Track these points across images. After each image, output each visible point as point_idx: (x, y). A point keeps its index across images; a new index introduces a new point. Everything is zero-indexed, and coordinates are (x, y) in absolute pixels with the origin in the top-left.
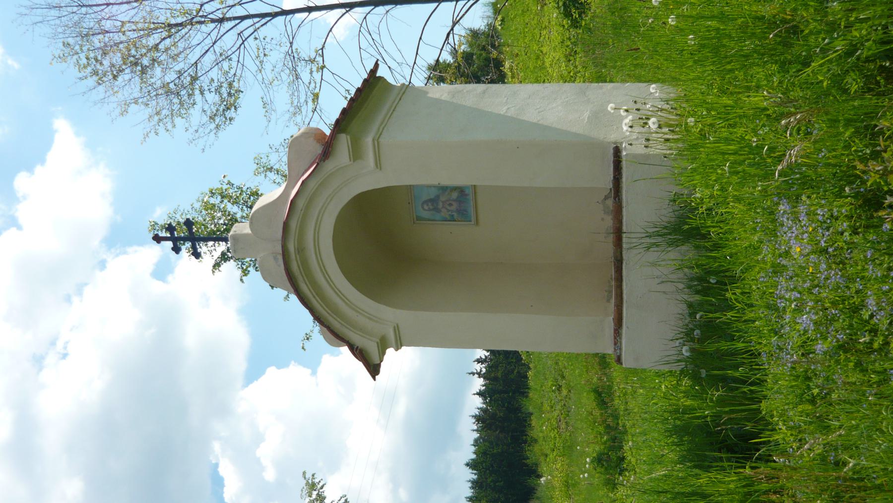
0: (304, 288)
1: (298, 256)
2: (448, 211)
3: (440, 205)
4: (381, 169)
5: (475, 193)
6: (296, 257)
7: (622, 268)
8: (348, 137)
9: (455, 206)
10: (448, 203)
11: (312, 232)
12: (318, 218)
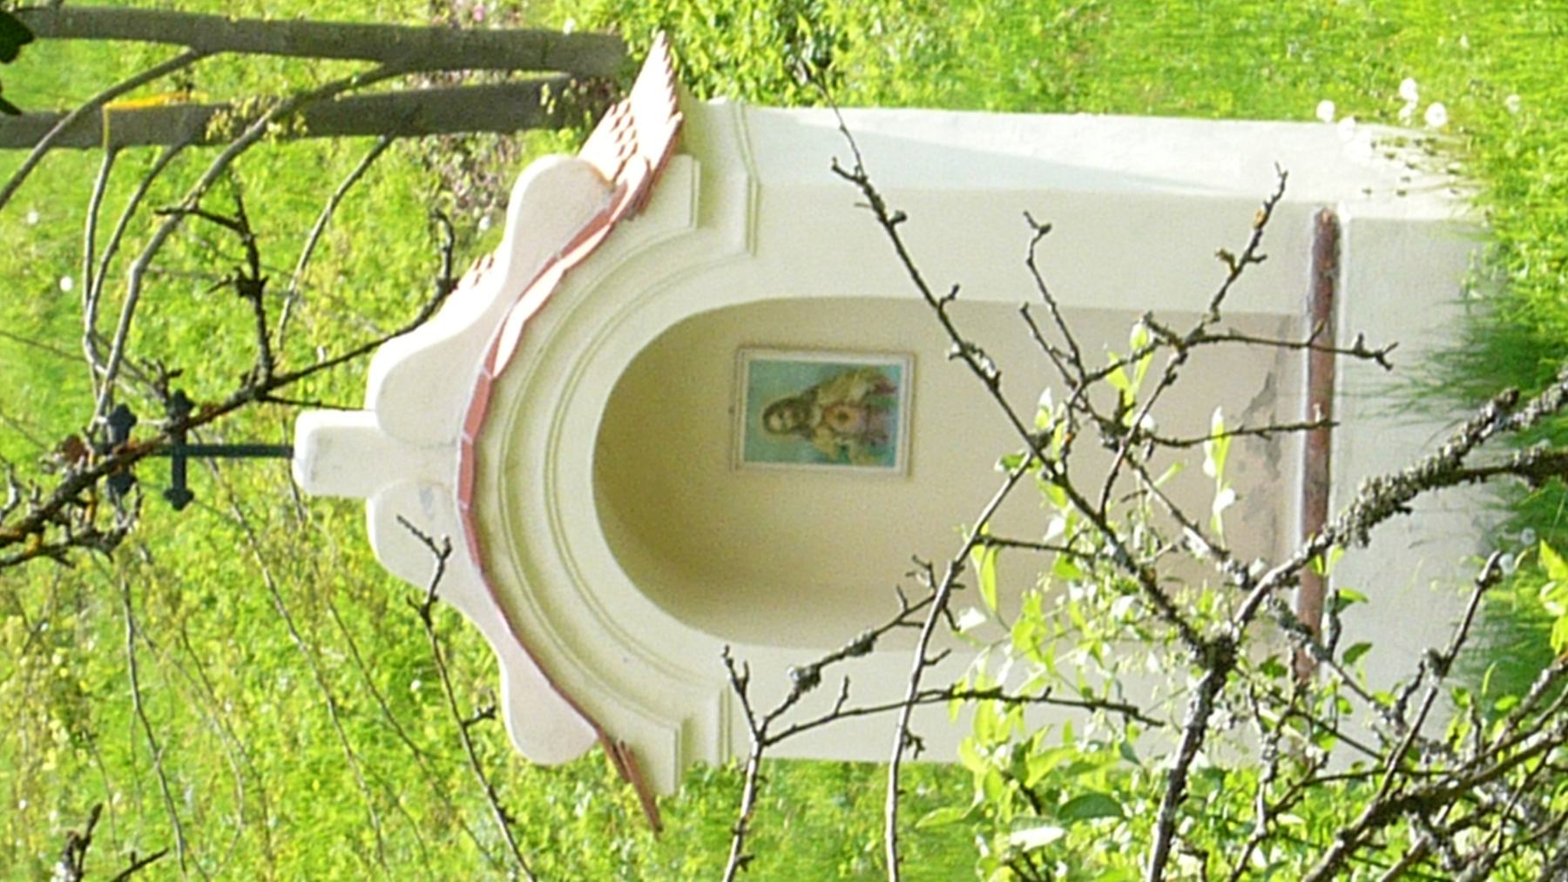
0: (506, 567)
1: (503, 481)
2: (834, 433)
3: (816, 419)
4: (754, 254)
5: (914, 396)
6: (499, 484)
7: (1326, 507)
8: (697, 165)
9: (856, 421)
10: (836, 411)
11: (549, 421)
12: (571, 378)
